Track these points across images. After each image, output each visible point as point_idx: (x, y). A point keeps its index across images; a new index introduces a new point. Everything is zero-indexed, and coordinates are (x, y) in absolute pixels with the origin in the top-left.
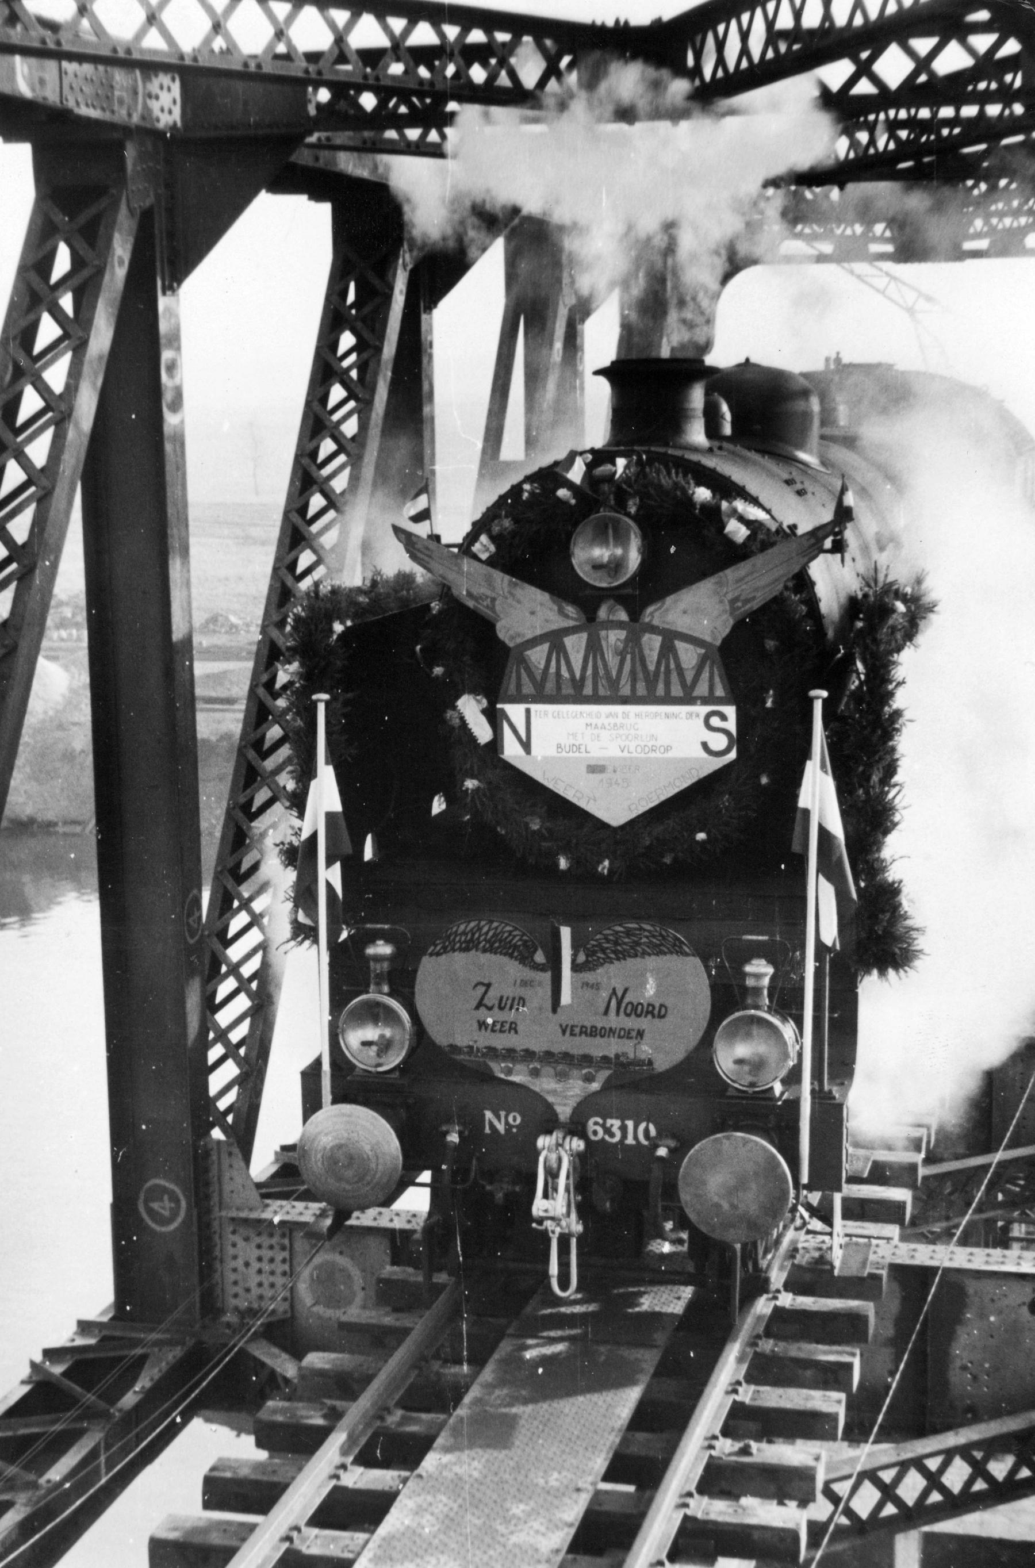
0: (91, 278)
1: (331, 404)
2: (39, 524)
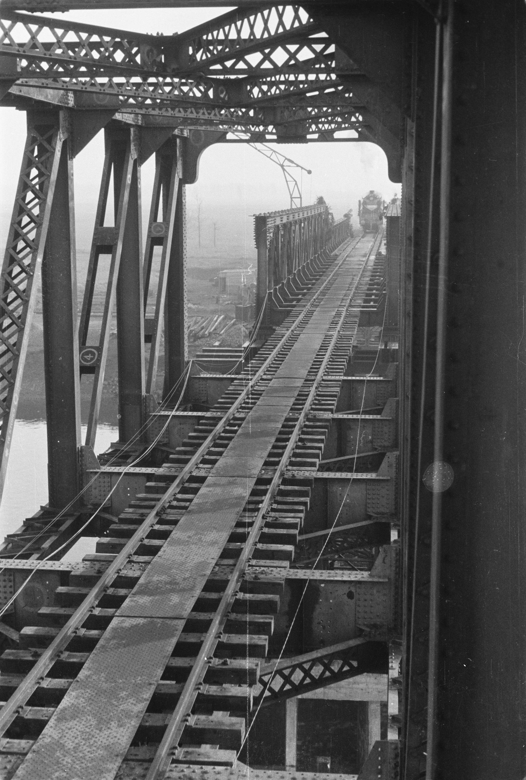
1: (27, 201)
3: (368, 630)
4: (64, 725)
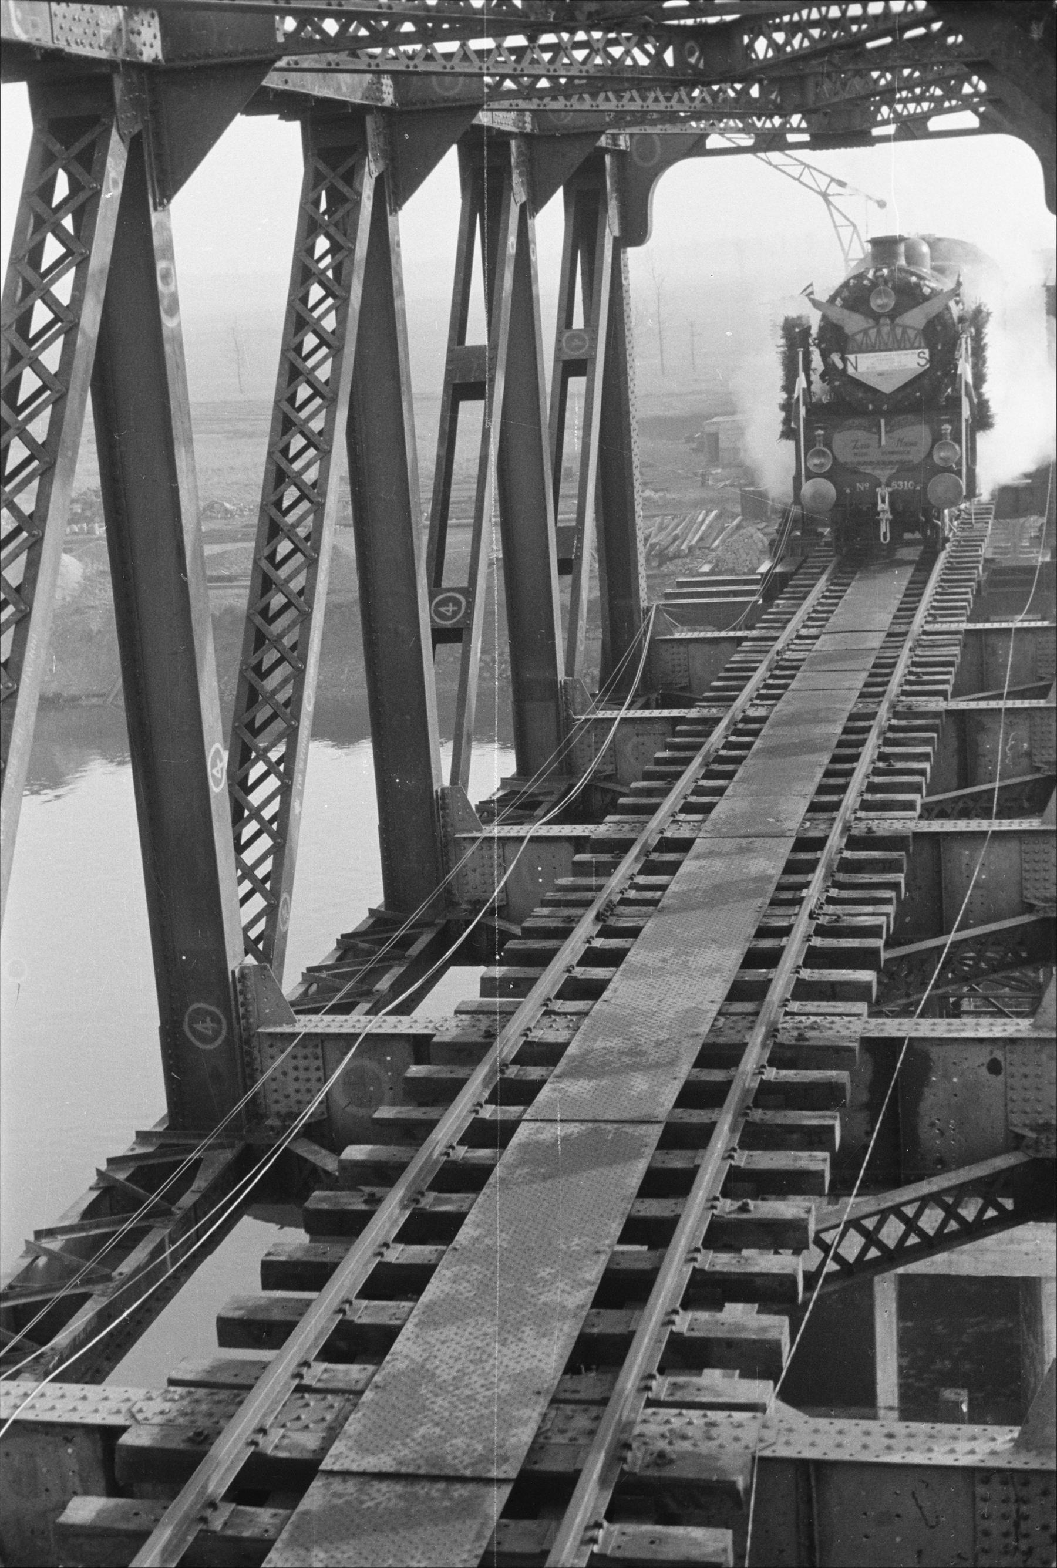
0: (88, 199)
1: (311, 303)
2: (56, 425)
3: (1034, 1135)
4: (433, 1336)
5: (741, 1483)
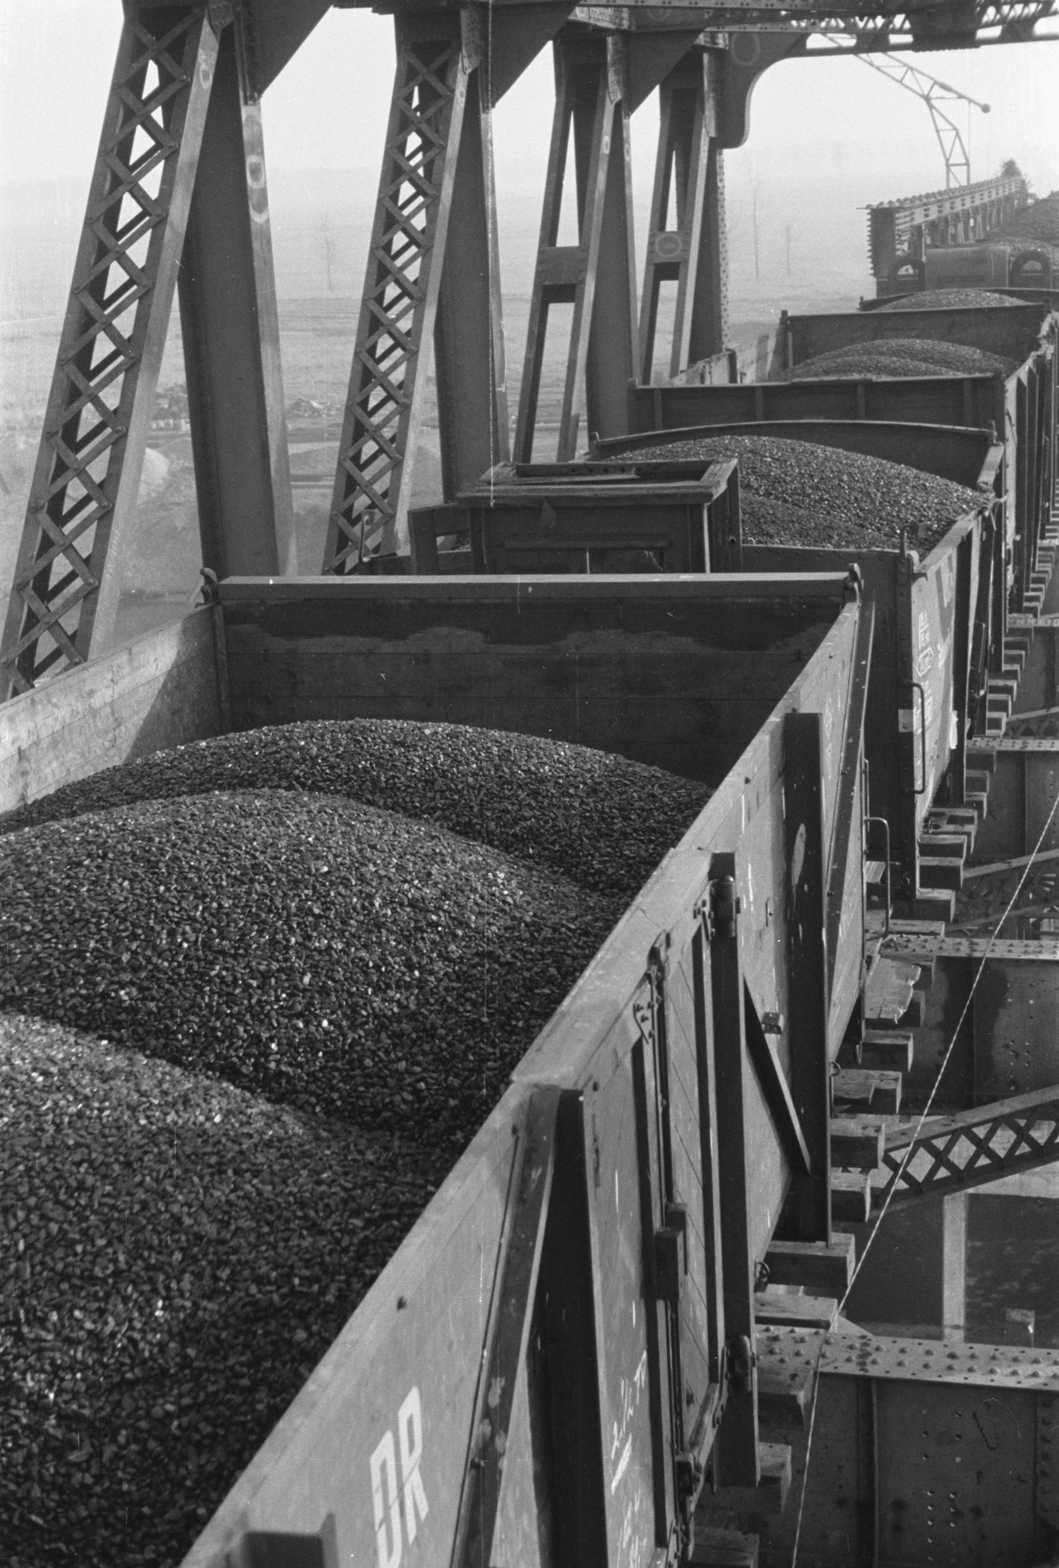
0: (179, 91)
1: (401, 200)
2: (141, 320)
5: (802, 1397)
